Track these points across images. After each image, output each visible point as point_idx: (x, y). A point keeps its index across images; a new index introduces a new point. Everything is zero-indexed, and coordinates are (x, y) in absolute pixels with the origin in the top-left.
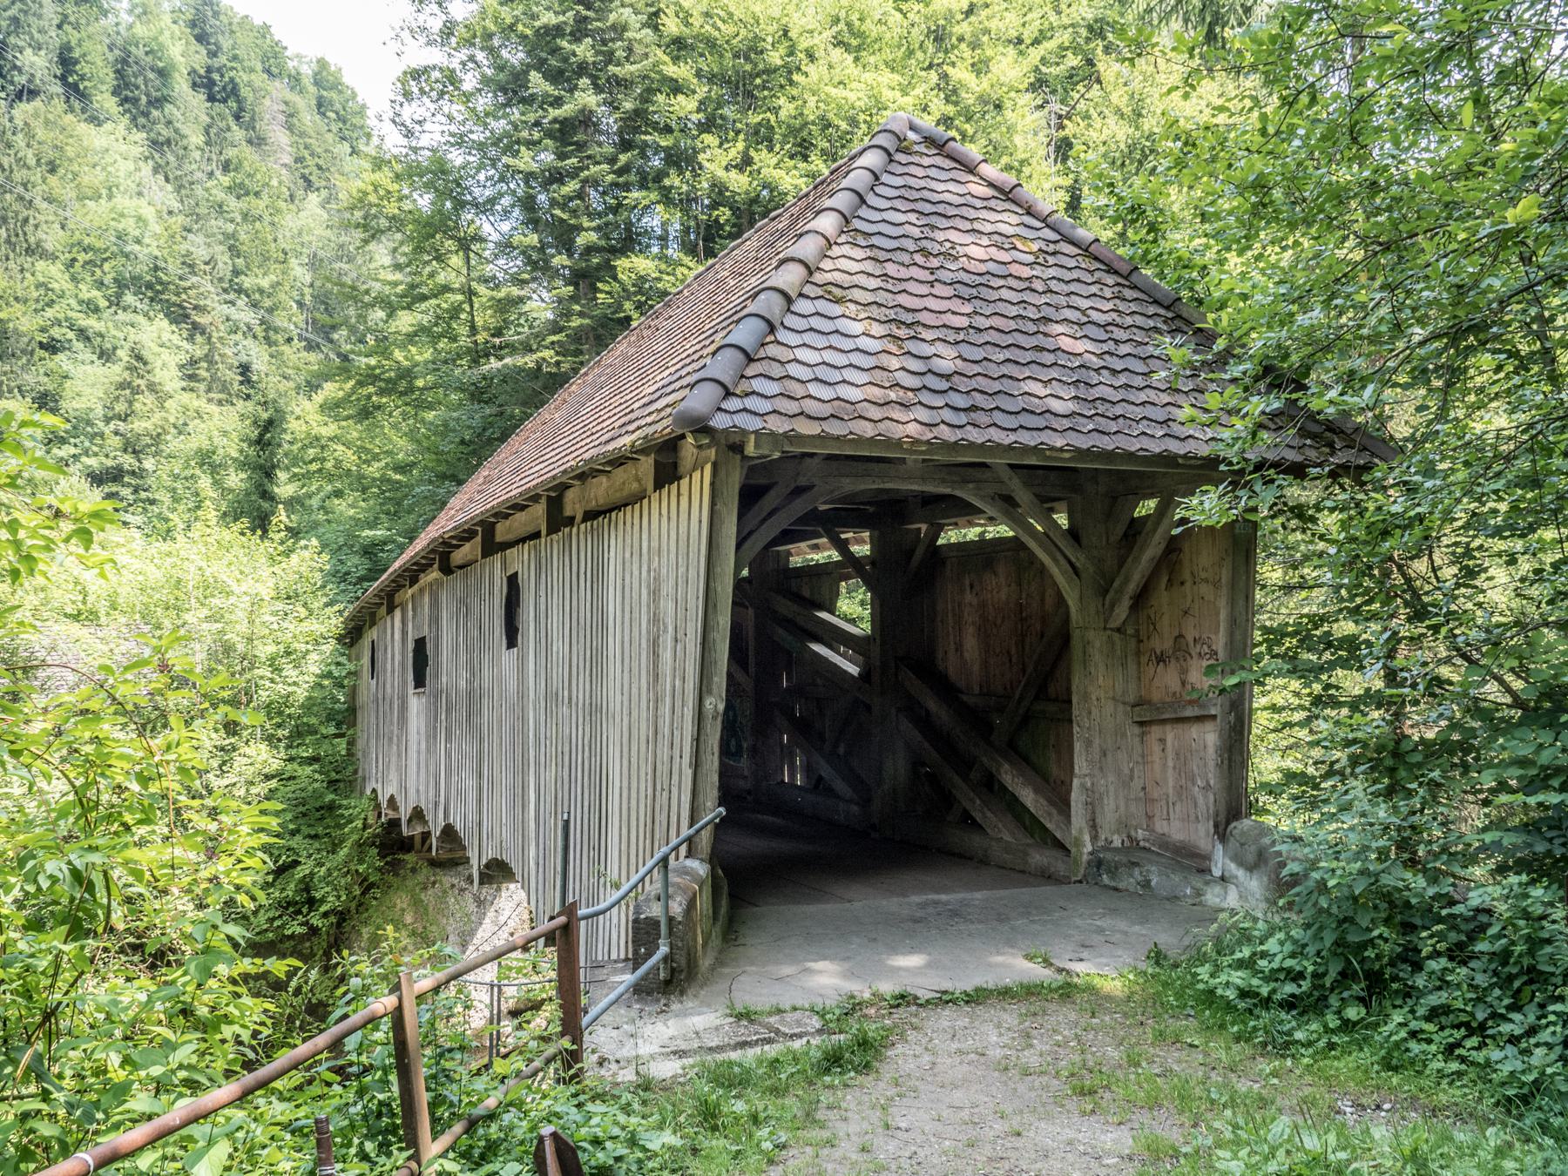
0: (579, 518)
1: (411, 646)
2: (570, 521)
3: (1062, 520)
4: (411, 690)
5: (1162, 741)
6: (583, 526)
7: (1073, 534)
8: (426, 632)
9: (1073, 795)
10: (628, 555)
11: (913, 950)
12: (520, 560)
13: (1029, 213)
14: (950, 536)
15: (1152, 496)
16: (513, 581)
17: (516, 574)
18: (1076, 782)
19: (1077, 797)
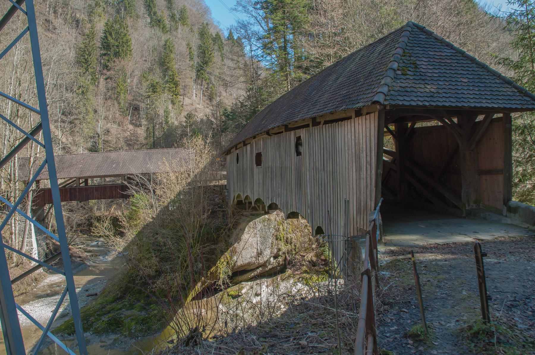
0: (322, 123)
1: (254, 155)
2: (319, 123)
3: (455, 120)
4: (255, 165)
5: (486, 180)
6: (324, 126)
7: (459, 125)
8: (261, 151)
9: (462, 194)
10: (346, 133)
11: (360, 253)
12: (303, 133)
13: (451, 49)
14: (418, 125)
15: (482, 114)
16: (299, 139)
17: (300, 137)
18: (463, 190)
19: (463, 195)
